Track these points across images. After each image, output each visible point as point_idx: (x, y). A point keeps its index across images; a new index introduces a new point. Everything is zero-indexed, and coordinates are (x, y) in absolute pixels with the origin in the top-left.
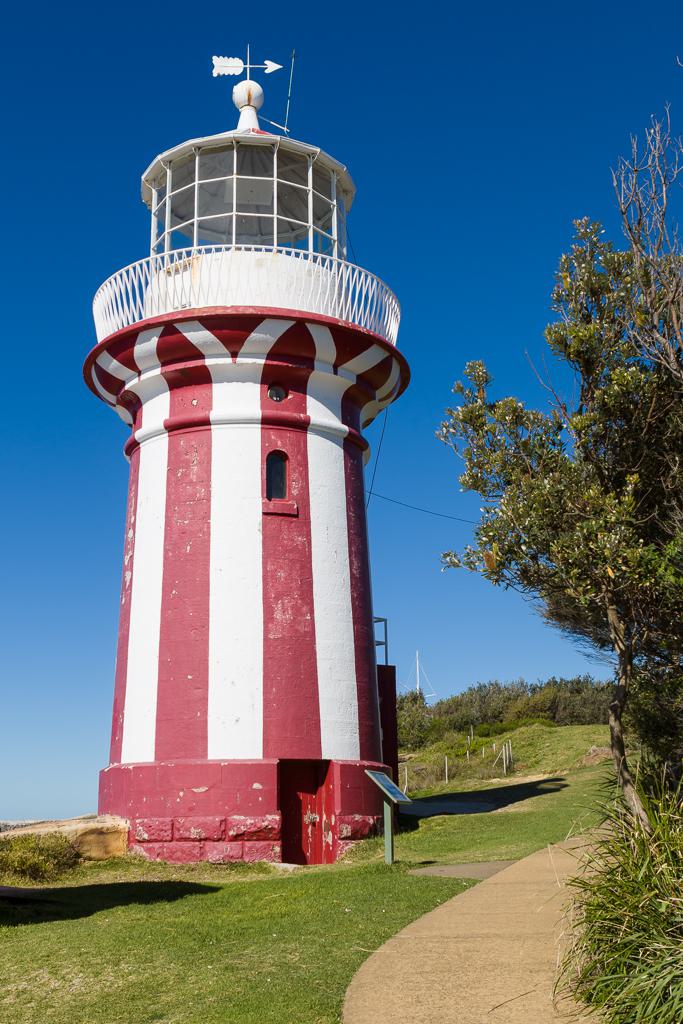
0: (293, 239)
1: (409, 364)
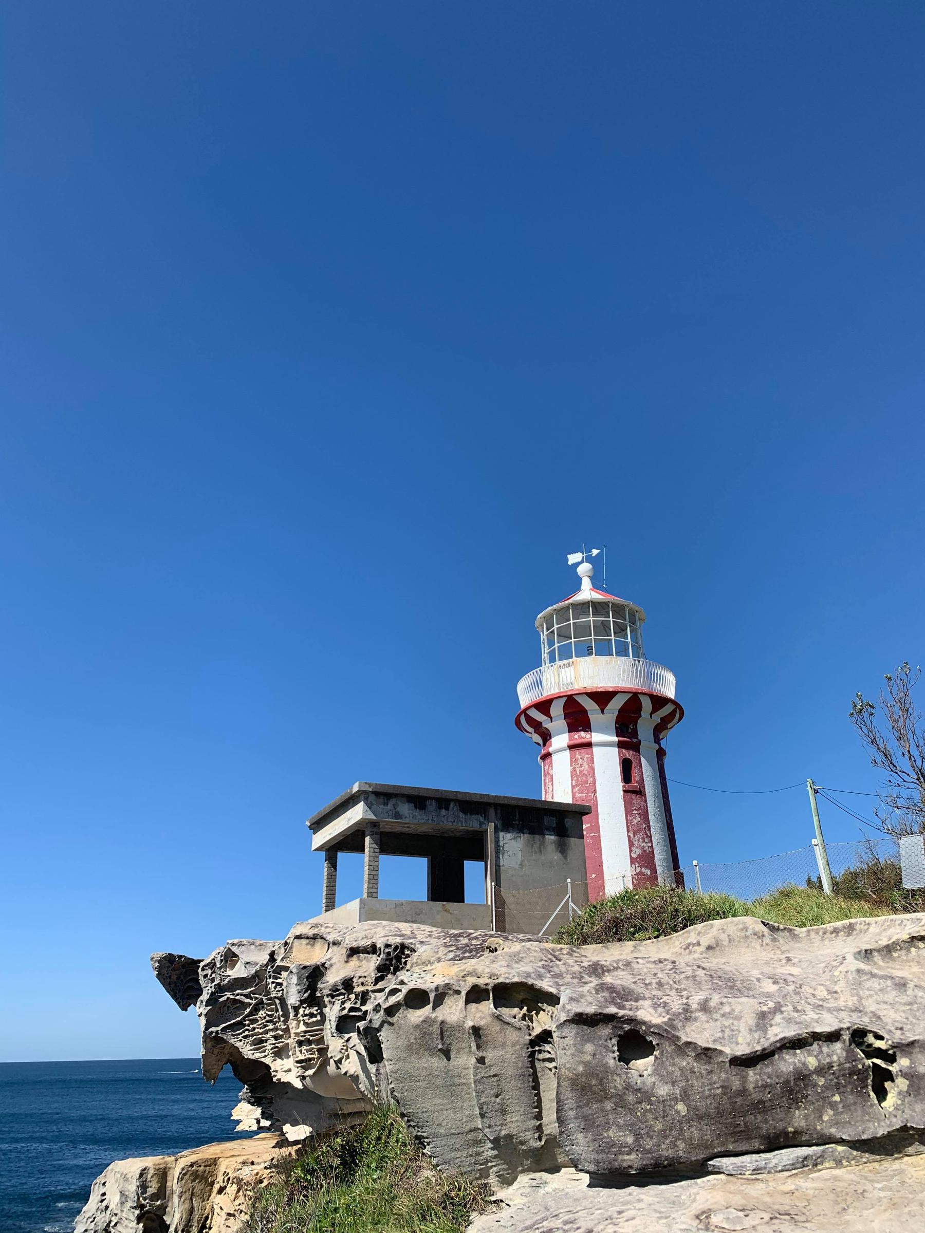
0: (622, 651)
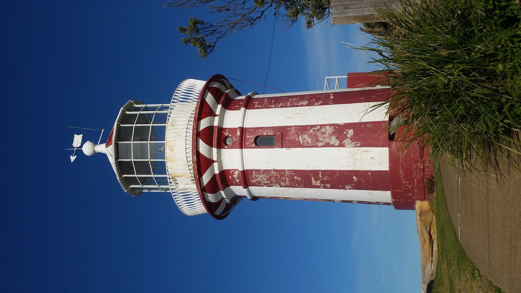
0: (163, 118)
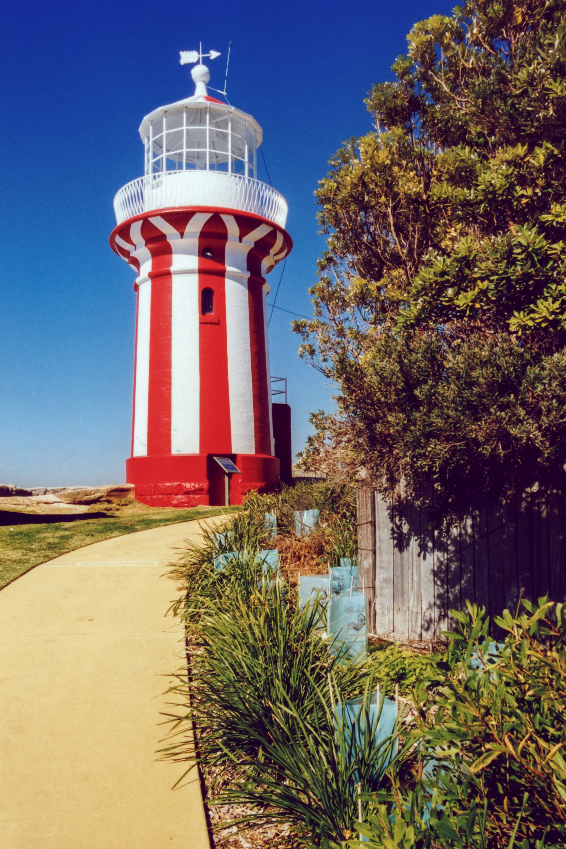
1: (292, 239)
